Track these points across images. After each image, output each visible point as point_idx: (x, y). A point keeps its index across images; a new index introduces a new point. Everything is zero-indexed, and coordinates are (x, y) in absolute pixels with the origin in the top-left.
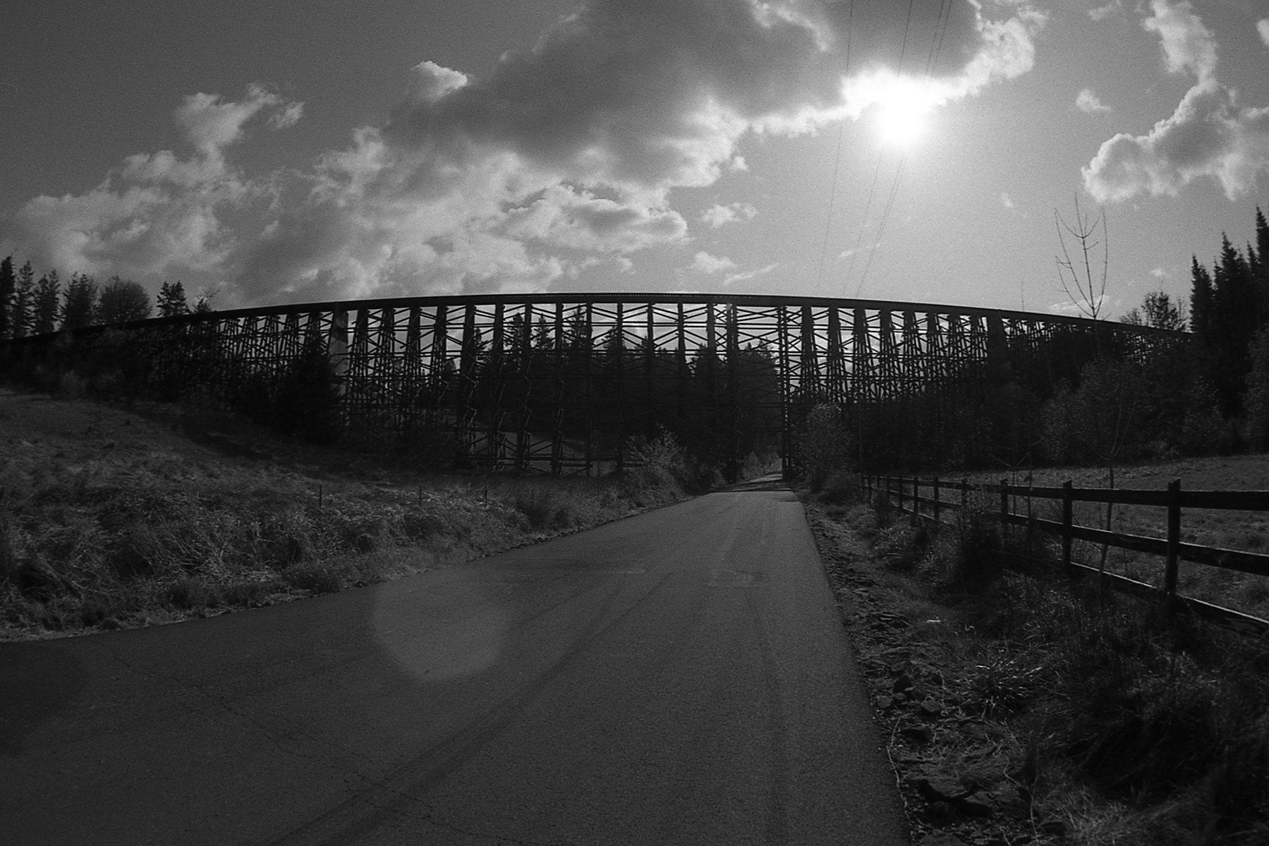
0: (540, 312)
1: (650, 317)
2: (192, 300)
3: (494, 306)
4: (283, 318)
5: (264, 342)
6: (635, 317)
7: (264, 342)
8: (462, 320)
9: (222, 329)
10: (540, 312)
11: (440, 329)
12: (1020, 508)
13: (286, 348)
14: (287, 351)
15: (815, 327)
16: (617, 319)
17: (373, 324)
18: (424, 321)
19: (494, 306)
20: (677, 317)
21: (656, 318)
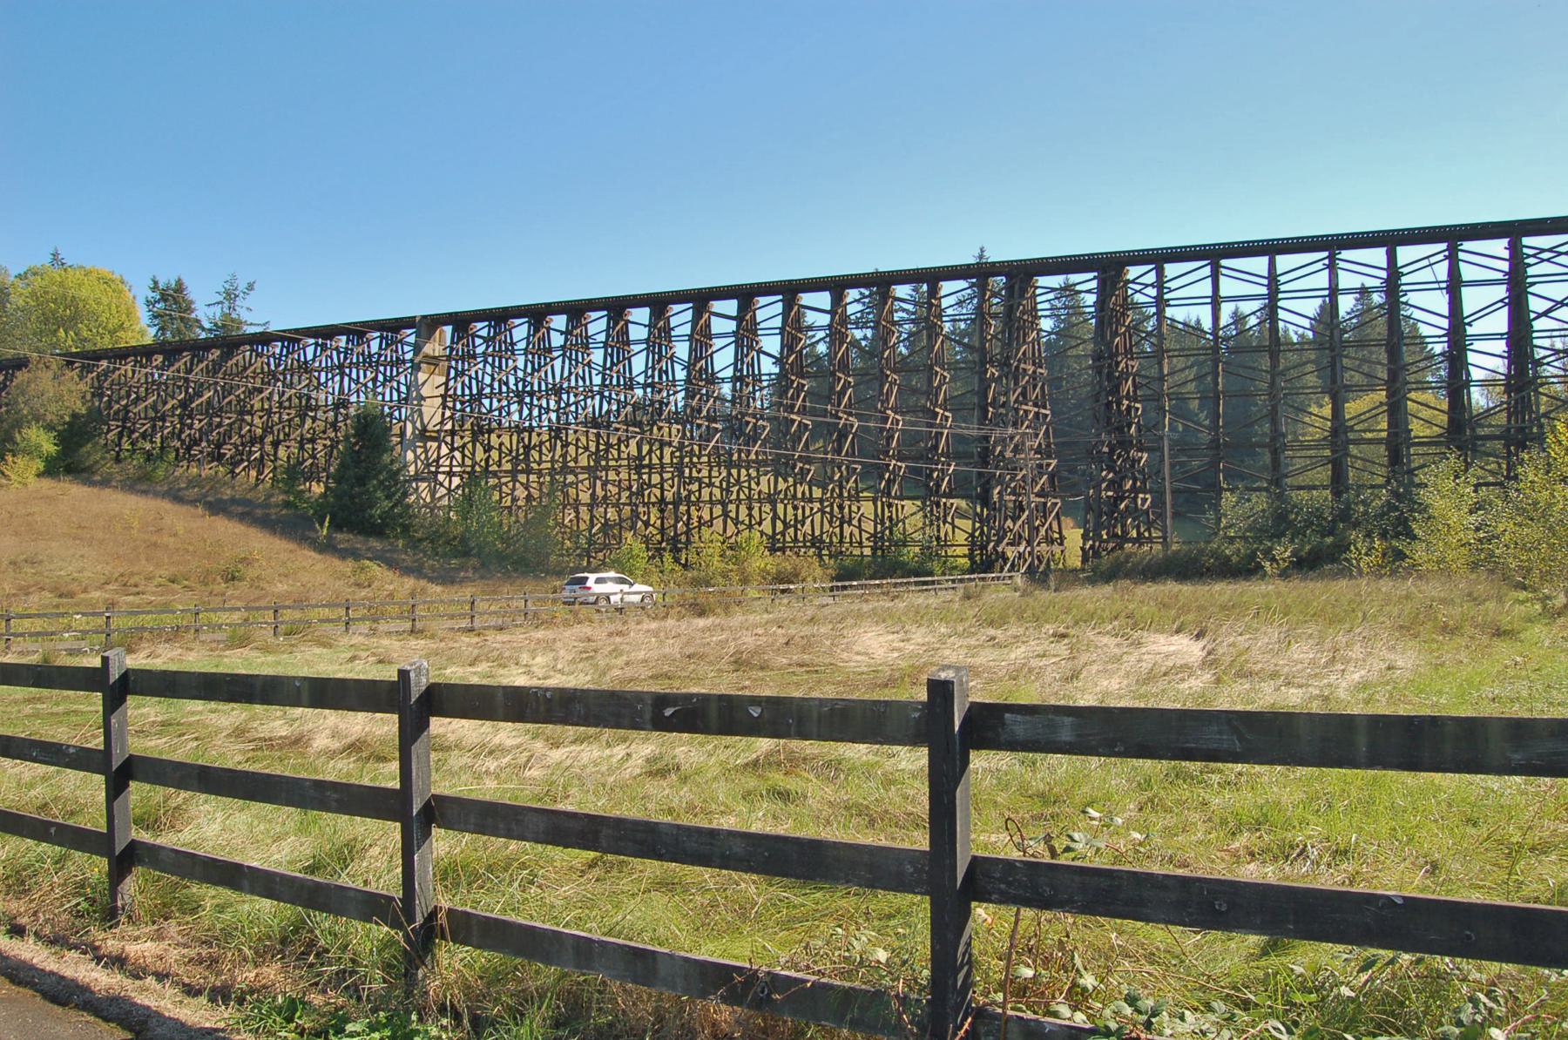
0: (1425, 262)
1: (1333, 278)
2: (206, 312)
3: (1505, 242)
4: (559, 322)
5: (529, 365)
6: (1189, 281)
7: (529, 365)
8: (778, 322)
9: (310, 356)
10: (1425, 262)
11: (746, 334)
12: (628, 598)
13: (570, 374)
14: (573, 378)
15: (1446, 339)
16: (1269, 286)
17: (638, 333)
18: (718, 325)
19: (1505, 242)
20: (1461, 255)
21: (1467, 272)
